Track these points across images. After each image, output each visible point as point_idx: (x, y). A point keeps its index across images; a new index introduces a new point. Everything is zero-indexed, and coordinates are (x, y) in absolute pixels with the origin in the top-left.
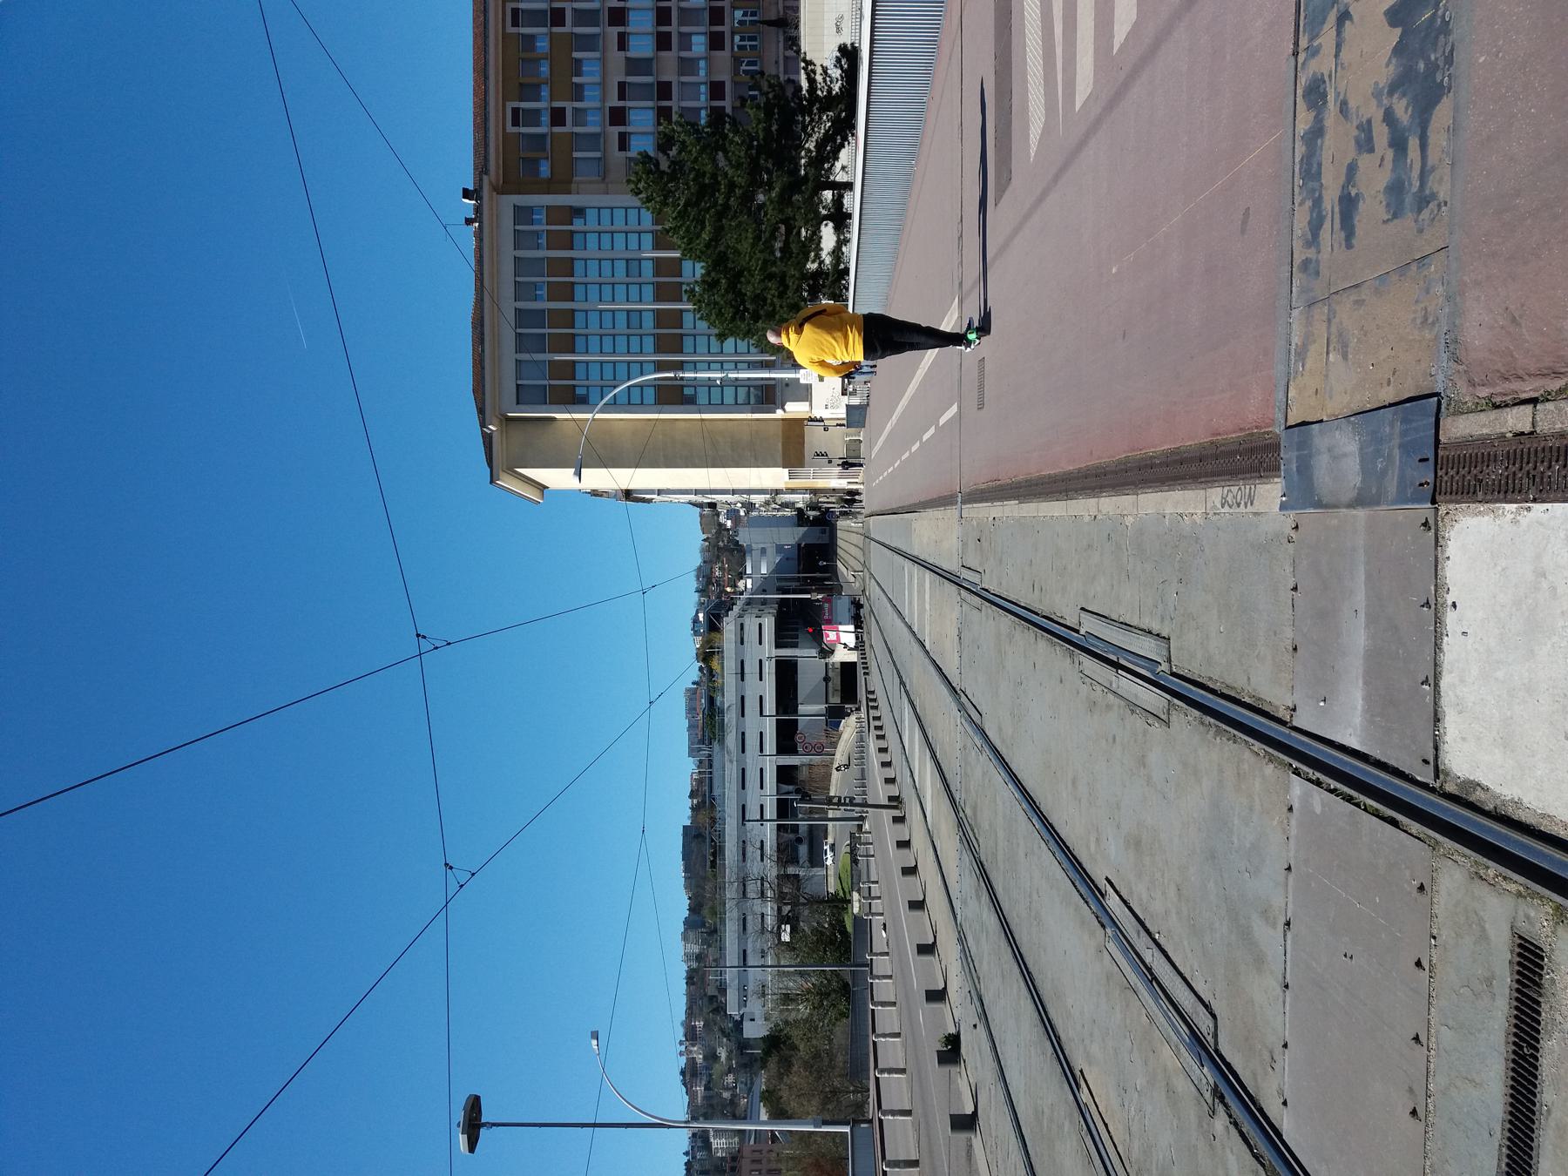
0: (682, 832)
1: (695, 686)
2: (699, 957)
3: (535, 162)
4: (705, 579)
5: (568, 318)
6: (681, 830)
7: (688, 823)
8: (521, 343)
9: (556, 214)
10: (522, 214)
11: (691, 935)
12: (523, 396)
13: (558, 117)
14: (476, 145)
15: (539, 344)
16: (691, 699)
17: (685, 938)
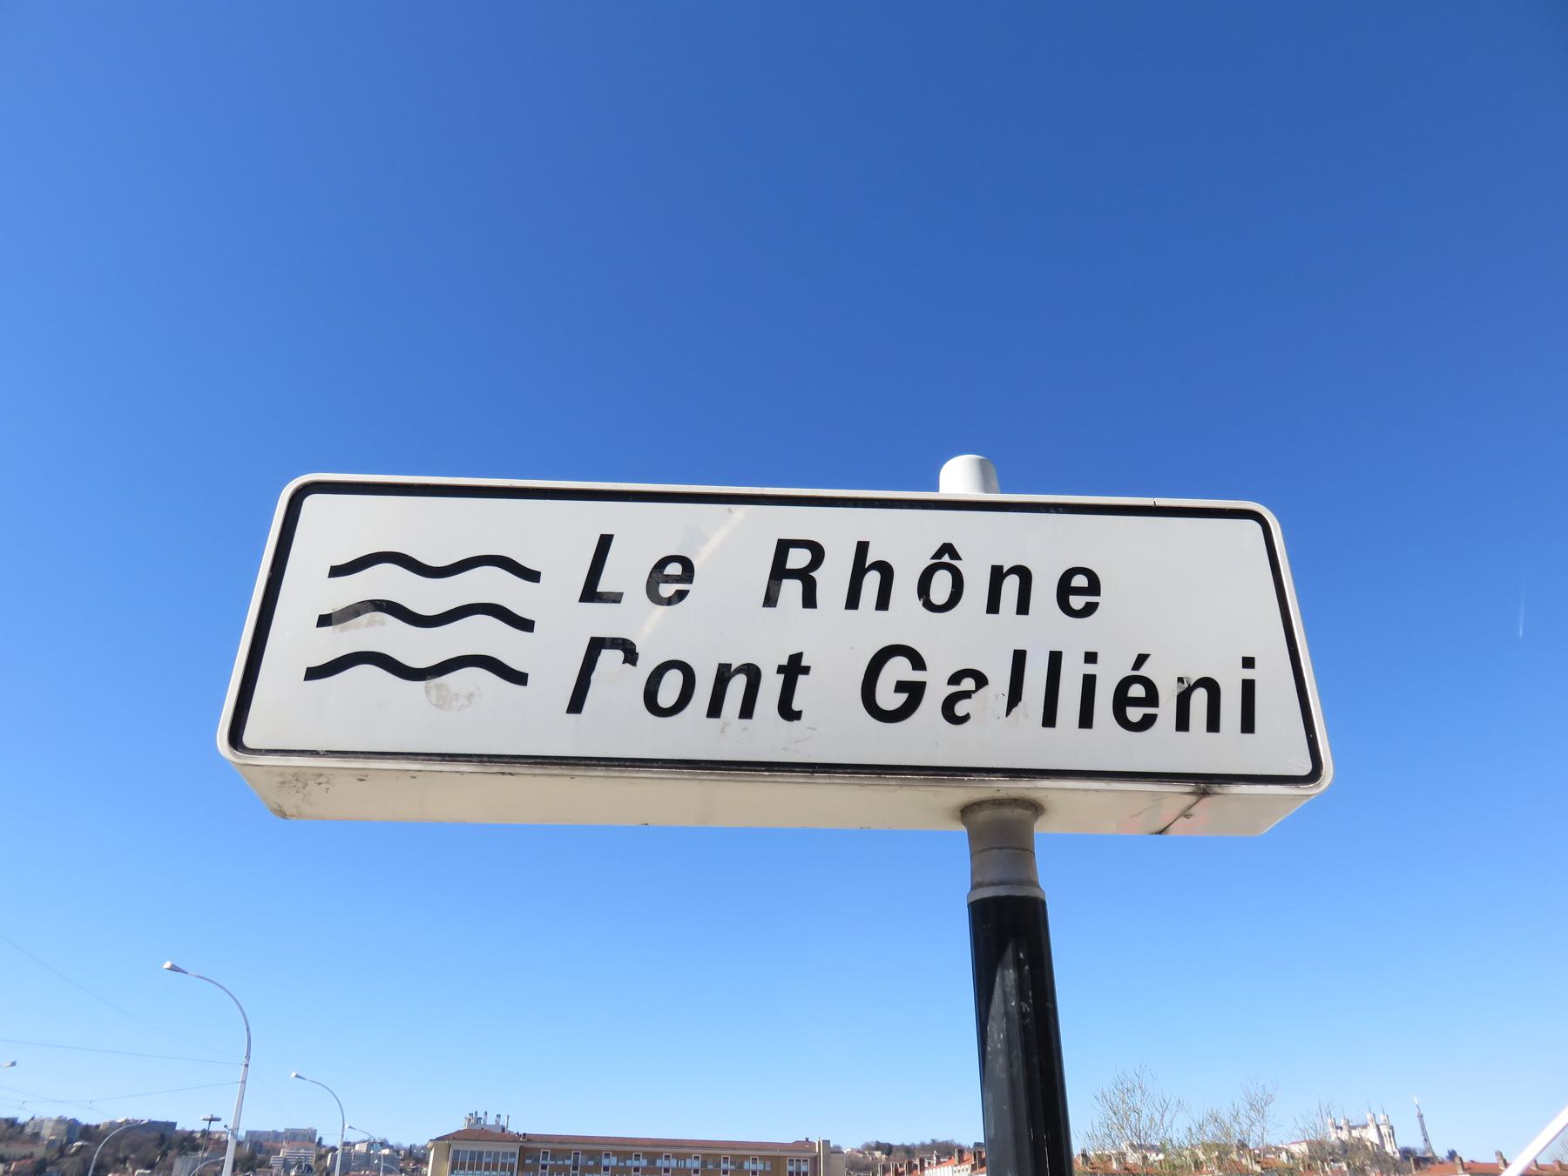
0: (170, 1121)
1: (317, 1140)
2: (36, 1136)
3: (530, 1158)
4: (421, 1156)
5: (479, 1168)
6: (171, 1120)
7: (178, 1128)
8: (473, 1153)
9: (512, 1165)
10: (513, 1155)
11: (63, 1127)
12: (456, 1152)
13: (544, 1167)
14: (541, 1136)
15: (472, 1158)
16: (305, 1136)
17: (60, 1121)
